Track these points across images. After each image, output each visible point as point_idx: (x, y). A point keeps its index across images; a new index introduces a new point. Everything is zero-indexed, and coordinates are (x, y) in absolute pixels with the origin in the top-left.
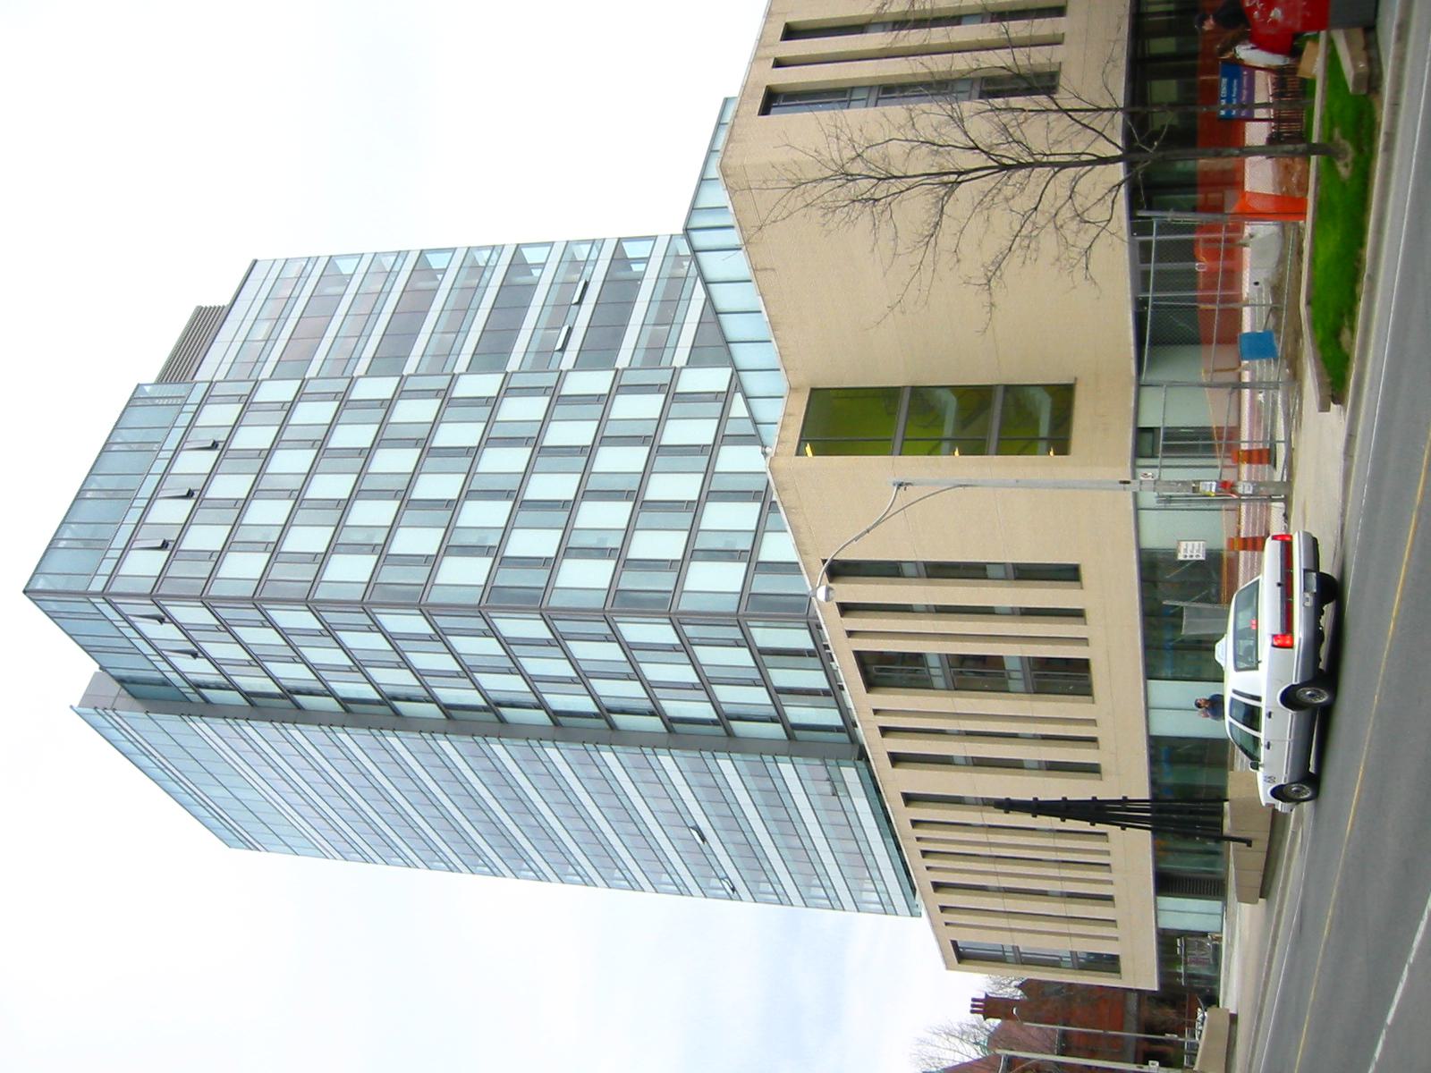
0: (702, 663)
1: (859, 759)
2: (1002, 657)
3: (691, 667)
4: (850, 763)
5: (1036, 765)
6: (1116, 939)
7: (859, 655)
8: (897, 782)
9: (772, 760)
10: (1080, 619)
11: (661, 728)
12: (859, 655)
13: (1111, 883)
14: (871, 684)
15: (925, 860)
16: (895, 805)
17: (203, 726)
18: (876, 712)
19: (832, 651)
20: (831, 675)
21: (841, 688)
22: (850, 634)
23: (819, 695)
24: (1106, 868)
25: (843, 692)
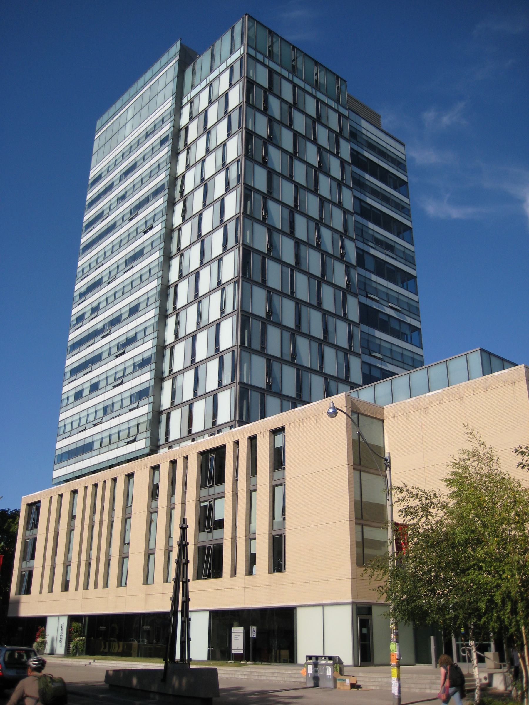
0: (208, 363)
1: (150, 450)
2: (223, 528)
3: (205, 357)
4: (148, 444)
5: (170, 545)
6: (41, 592)
7: (223, 447)
8: (141, 470)
9: (150, 402)
10: (64, 589)
11: (168, 343)
12: (223, 447)
13: (77, 589)
14: (204, 455)
15: (246, 439)
16: (127, 468)
17: (170, 104)
18: (186, 458)
19: (217, 435)
20: (201, 433)
21: (193, 440)
22: (237, 443)
23: (166, 436)
24: (166, 580)
25: (191, 441)
